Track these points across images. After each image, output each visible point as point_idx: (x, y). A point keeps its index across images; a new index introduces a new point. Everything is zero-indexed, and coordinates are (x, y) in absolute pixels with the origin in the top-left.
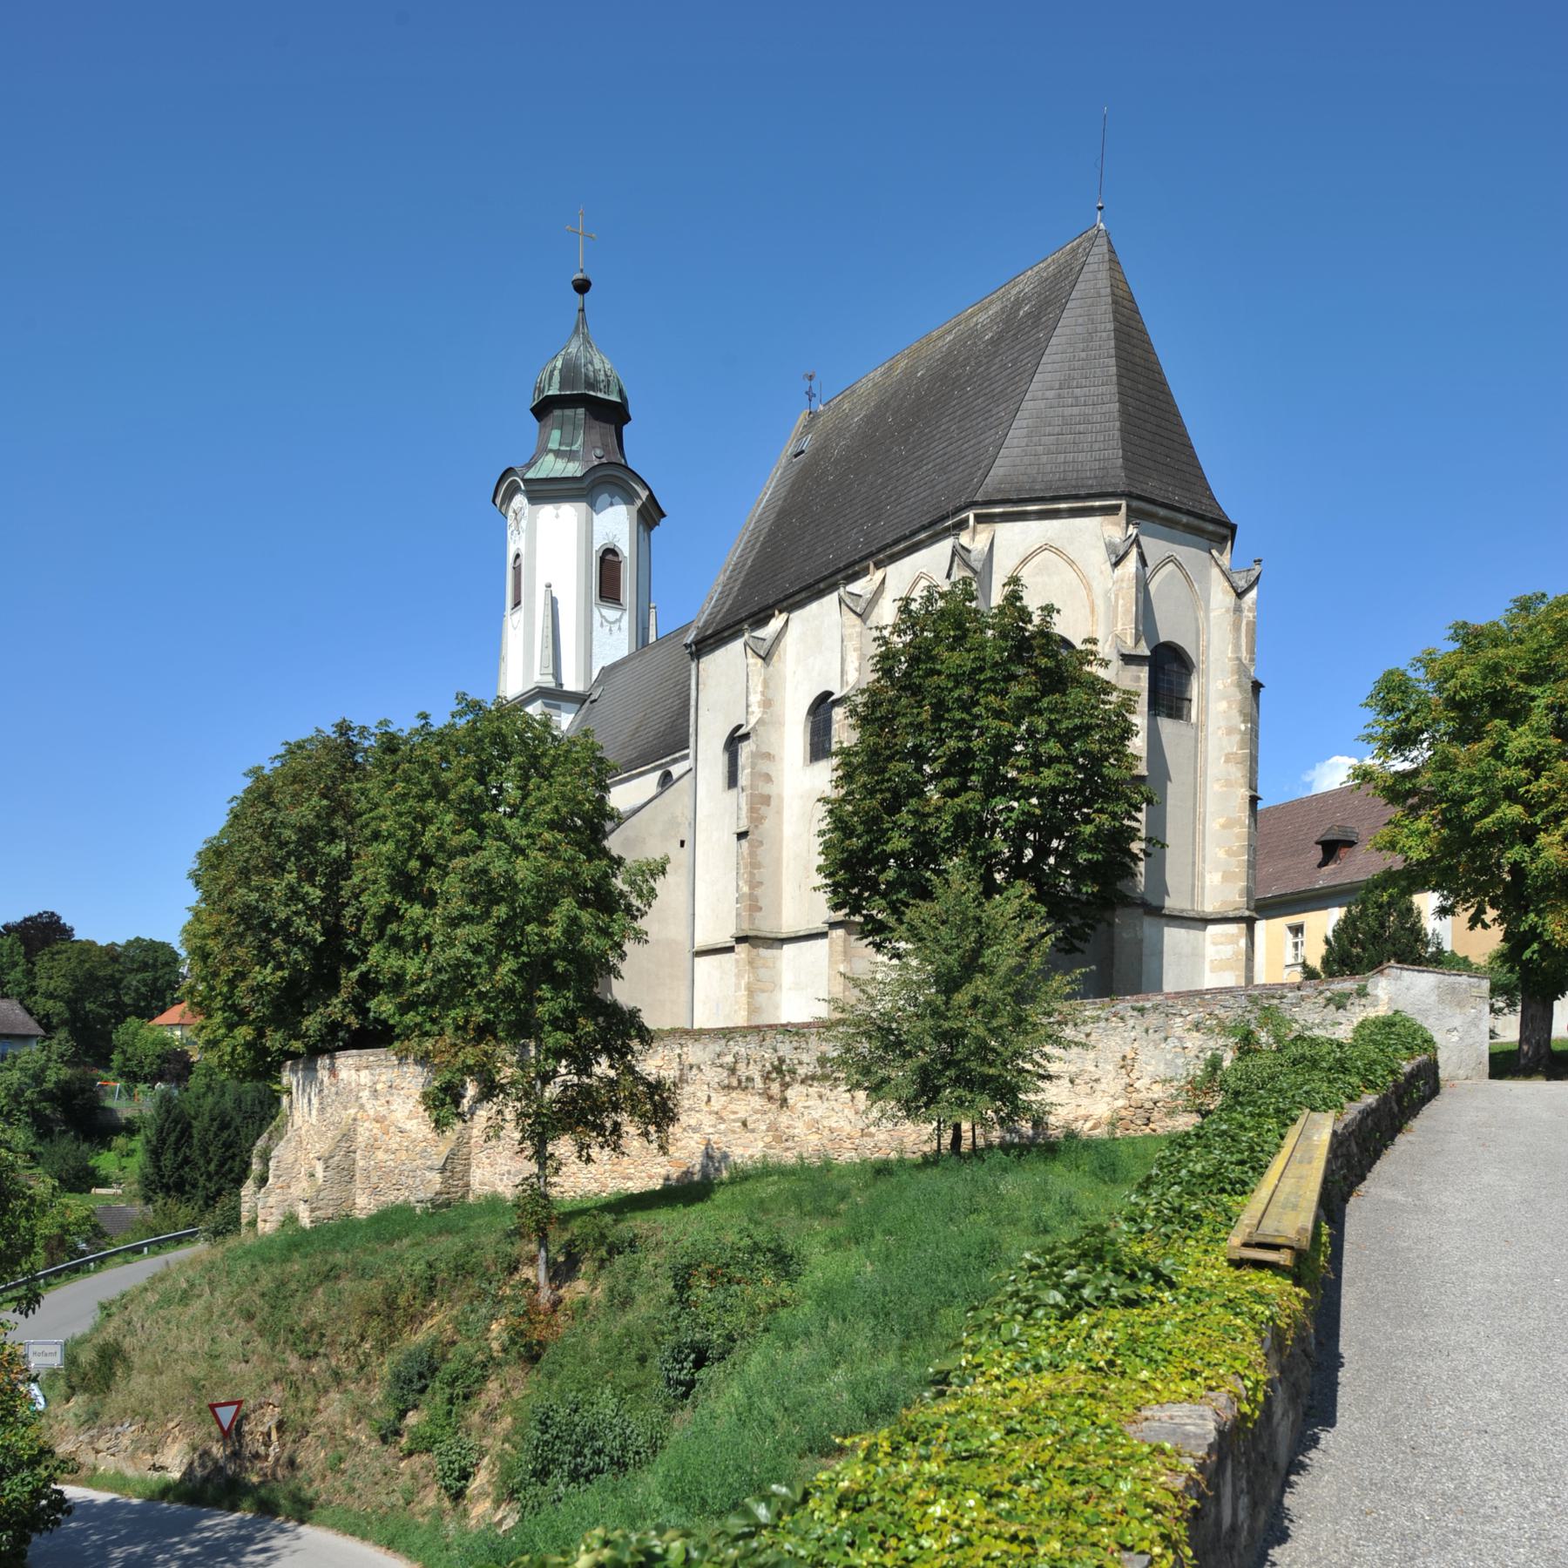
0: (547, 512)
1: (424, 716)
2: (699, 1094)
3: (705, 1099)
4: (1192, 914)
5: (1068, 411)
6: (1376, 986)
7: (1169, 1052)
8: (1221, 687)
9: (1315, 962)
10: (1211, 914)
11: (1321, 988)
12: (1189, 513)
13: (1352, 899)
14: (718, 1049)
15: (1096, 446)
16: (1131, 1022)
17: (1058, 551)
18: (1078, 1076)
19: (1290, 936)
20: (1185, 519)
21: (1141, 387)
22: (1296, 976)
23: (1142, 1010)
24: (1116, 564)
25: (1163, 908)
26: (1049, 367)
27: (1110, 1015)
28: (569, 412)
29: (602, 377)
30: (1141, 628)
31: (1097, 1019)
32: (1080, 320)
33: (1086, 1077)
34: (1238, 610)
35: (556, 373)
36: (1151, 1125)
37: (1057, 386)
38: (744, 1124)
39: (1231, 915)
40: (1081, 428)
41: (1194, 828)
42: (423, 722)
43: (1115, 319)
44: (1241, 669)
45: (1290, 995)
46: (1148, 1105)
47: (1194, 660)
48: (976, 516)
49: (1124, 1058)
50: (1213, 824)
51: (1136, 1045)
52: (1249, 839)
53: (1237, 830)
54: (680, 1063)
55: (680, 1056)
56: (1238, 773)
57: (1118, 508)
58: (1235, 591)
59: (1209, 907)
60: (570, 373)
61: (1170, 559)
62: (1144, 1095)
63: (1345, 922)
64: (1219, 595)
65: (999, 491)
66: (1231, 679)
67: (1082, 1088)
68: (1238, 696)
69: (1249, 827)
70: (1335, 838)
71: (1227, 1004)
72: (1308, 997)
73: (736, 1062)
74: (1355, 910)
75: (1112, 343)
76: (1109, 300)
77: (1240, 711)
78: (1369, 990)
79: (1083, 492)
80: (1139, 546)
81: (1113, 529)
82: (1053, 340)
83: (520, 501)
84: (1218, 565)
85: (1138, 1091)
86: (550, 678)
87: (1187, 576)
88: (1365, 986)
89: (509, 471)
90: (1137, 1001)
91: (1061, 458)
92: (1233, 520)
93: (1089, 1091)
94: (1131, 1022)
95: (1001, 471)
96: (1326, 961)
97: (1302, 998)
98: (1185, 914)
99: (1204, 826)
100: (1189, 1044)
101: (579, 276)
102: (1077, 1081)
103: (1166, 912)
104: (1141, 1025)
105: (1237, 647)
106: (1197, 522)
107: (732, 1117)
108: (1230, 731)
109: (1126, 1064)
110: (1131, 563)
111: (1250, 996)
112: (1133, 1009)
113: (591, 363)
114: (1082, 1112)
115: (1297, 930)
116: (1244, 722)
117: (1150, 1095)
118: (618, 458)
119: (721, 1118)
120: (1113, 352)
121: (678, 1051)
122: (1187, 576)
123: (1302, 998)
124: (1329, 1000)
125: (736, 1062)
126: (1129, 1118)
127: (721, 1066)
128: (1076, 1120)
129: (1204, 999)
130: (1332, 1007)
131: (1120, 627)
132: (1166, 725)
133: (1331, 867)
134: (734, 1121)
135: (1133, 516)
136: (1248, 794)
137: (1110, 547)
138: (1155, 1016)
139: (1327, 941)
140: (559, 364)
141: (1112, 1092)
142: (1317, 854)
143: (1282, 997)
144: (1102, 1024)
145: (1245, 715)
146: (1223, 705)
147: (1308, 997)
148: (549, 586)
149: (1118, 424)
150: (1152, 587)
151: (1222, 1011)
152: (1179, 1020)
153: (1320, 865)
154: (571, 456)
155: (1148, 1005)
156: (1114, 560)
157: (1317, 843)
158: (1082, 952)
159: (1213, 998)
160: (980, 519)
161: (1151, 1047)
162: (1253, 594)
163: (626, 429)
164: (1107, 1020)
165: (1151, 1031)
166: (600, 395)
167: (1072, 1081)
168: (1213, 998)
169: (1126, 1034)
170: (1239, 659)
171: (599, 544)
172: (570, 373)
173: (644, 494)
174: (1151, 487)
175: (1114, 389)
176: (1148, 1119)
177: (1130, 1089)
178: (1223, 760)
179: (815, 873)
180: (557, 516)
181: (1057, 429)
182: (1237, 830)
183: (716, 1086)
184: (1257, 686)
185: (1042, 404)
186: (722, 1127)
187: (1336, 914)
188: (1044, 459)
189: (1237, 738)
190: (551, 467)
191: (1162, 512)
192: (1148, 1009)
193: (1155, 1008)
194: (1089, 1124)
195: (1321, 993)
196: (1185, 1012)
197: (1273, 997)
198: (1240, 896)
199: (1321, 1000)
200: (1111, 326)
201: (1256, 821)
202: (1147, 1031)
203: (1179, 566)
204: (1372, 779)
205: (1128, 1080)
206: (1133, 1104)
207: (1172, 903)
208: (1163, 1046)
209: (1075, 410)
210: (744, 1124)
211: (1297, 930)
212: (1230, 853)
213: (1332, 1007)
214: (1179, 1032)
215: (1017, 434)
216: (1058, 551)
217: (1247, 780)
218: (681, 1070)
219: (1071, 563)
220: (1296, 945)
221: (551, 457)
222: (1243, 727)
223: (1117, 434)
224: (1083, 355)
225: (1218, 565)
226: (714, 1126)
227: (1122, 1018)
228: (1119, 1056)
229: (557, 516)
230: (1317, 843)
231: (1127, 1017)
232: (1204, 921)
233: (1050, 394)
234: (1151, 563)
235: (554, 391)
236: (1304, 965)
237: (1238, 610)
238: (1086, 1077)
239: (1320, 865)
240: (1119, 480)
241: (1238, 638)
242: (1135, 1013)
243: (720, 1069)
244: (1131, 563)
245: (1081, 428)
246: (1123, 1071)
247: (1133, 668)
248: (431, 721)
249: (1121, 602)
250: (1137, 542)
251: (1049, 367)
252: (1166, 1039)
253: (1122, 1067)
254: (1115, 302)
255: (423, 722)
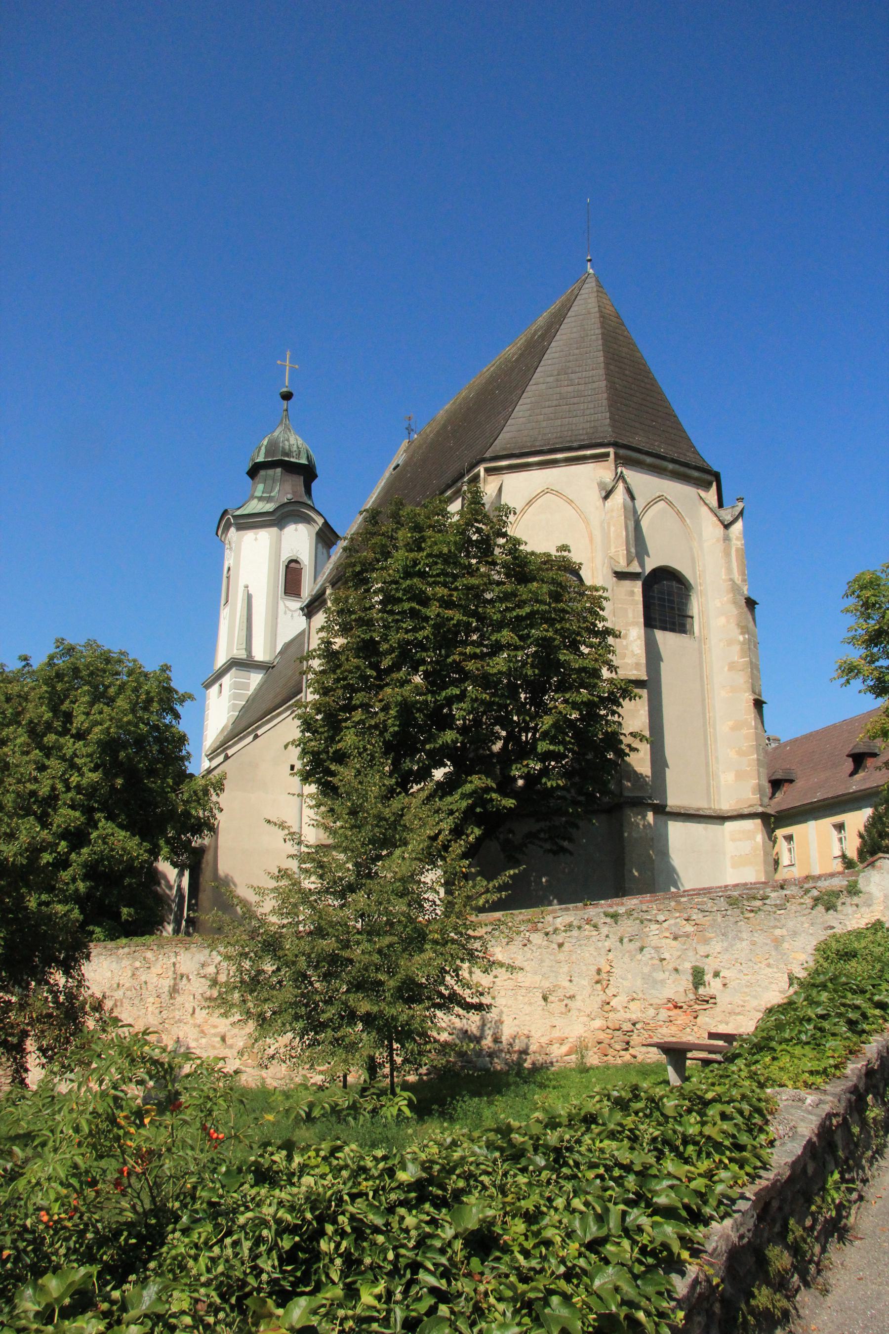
0: (249, 536)
1: (25, 659)
2: (187, 1005)
3: (191, 1011)
4: (708, 813)
5: (564, 390)
6: (868, 881)
7: (646, 964)
8: (719, 605)
9: (852, 854)
10: (728, 811)
11: (806, 886)
12: (673, 461)
13: (877, 800)
14: (202, 959)
15: (588, 412)
16: (605, 930)
17: (558, 494)
18: (551, 992)
19: (835, 833)
20: (671, 466)
21: (627, 372)
22: (838, 866)
23: (615, 916)
24: (606, 497)
25: (666, 806)
26: (550, 362)
27: (583, 923)
28: (270, 472)
29: (295, 448)
30: (633, 550)
31: (569, 927)
32: (575, 330)
33: (560, 993)
34: (727, 539)
35: (263, 449)
36: (631, 1051)
37: (555, 373)
38: (223, 1039)
39: (746, 811)
40: (576, 400)
41: (705, 731)
42: (24, 663)
43: (603, 327)
44: (735, 588)
45: (773, 895)
46: (627, 1026)
47: (692, 582)
48: (488, 471)
49: (599, 971)
50: (723, 727)
51: (611, 956)
52: (757, 740)
53: (745, 731)
54: (174, 973)
55: (174, 964)
56: (742, 679)
57: (607, 455)
58: (722, 522)
59: (725, 805)
60: (272, 448)
61: (660, 498)
62: (621, 1015)
63: (873, 818)
64: (710, 527)
65: (504, 449)
66: (727, 597)
67: (556, 1006)
68: (733, 611)
69: (756, 728)
70: (861, 751)
71: (705, 907)
72: (794, 897)
73: (218, 973)
74: (882, 809)
75: (600, 342)
76: (598, 315)
77: (738, 625)
78: (861, 885)
79: (575, 444)
80: (625, 481)
81: (604, 472)
82: (553, 344)
83: (233, 530)
84: (706, 504)
85: (613, 1010)
86: (244, 652)
87: (678, 513)
88: (856, 882)
89: (225, 512)
90: (611, 906)
91: (559, 422)
92: (715, 468)
93: (563, 1010)
94: (605, 930)
95: (508, 436)
96: (861, 853)
97: (787, 899)
98: (701, 813)
99: (715, 729)
100: (666, 955)
101: (285, 390)
102: (551, 998)
103: (668, 809)
104: (615, 934)
105: (729, 570)
106: (682, 469)
107: (213, 1031)
108: (730, 643)
109: (601, 978)
110: (620, 494)
111: (729, 897)
112: (607, 915)
113: (288, 440)
114: (556, 1034)
115: (840, 827)
116: (743, 633)
117: (628, 1016)
118: (305, 499)
119: (202, 1032)
120: (601, 348)
121: (173, 960)
122: (678, 513)
123: (787, 899)
124: (817, 900)
125: (218, 973)
126: (607, 1041)
127: (204, 977)
128: (551, 1043)
129: (679, 903)
130: (821, 908)
131: (613, 550)
132: (665, 639)
133: (861, 775)
134: (215, 1035)
135: (623, 460)
136: (752, 697)
137: (601, 485)
138: (629, 922)
139: (861, 836)
140: (265, 442)
141: (588, 1012)
142: (849, 765)
143: (765, 898)
144: (575, 933)
145: (742, 628)
146: (722, 620)
147: (794, 897)
148: (247, 587)
149: (605, 395)
150: (644, 523)
151: (701, 915)
152: (654, 927)
153: (852, 774)
154: (269, 499)
155: (622, 910)
156: (604, 494)
157: (848, 756)
158: (571, 854)
159: (689, 901)
160: (488, 471)
161: (626, 959)
162: (738, 526)
163: (315, 485)
164: (579, 928)
165: (626, 940)
166: (292, 460)
167: (545, 999)
168: (689, 901)
169: (600, 944)
170: (732, 580)
171: (285, 557)
172: (272, 448)
173: (320, 521)
174: (637, 440)
175: (602, 372)
176: (628, 1043)
177: (607, 1007)
178: (726, 669)
179: (291, 778)
180: (256, 539)
181: (555, 403)
182: (745, 731)
183: (200, 997)
184: (751, 604)
185: (543, 386)
186: (203, 1041)
187: (867, 812)
188: (544, 424)
189: (736, 648)
190: (255, 506)
191: (649, 460)
192: (621, 915)
193: (629, 913)
194: (564, 1049)
195: (807, 892)
196: (661, 918)
197: (754, 898)
198: (753, 794)
199: (808, 900)
200: (599, 331)
201: (762, 722)
202: (621, 941)
203: (670, 503)
204: (859, 672)
205: (604, 997)
206: (610, 1025)
207: (674, 800)
208: (639, 957)
209: (570, 389)
210: (223, 1039)
211: (840, 827)
212: (740, 753)
213: (821, 908)
214: (654, 941)
215: (522, 410)
216: (558, 494)
217: (749, 685)
218: (175, 979)
219: (570, 502)
220: (840, 840)
221: (256, 501)
222: (741, 638)
223: (605, 402)
224: (577, 351)
225: (706, 504)
226: (197, 1040)
227: (595, 926)
228: (593, 969)
229: (256, 539)
230: (848, 756)
231: (601, 926)
232: (721, 818)
233: (551, 379)
234: (640, 504)
235: (261, 459)
236: (844, 856)
237: (727, 539)
238: (560, 993)
239: (852, 774)
240: (606, 432)
241: (729, 562)
242: (608, 920)
243: (203, 980)
244: (620, 494)
245: (576, 400)
246: (599, 986)
247: (627, 583)
248: (31, 662)
249: (612, 529)
250: (621, 477)
251: (550, 362)
252: (642, 949)
253: (597, 982)
254: (601, 316)
255: (24, 663)
